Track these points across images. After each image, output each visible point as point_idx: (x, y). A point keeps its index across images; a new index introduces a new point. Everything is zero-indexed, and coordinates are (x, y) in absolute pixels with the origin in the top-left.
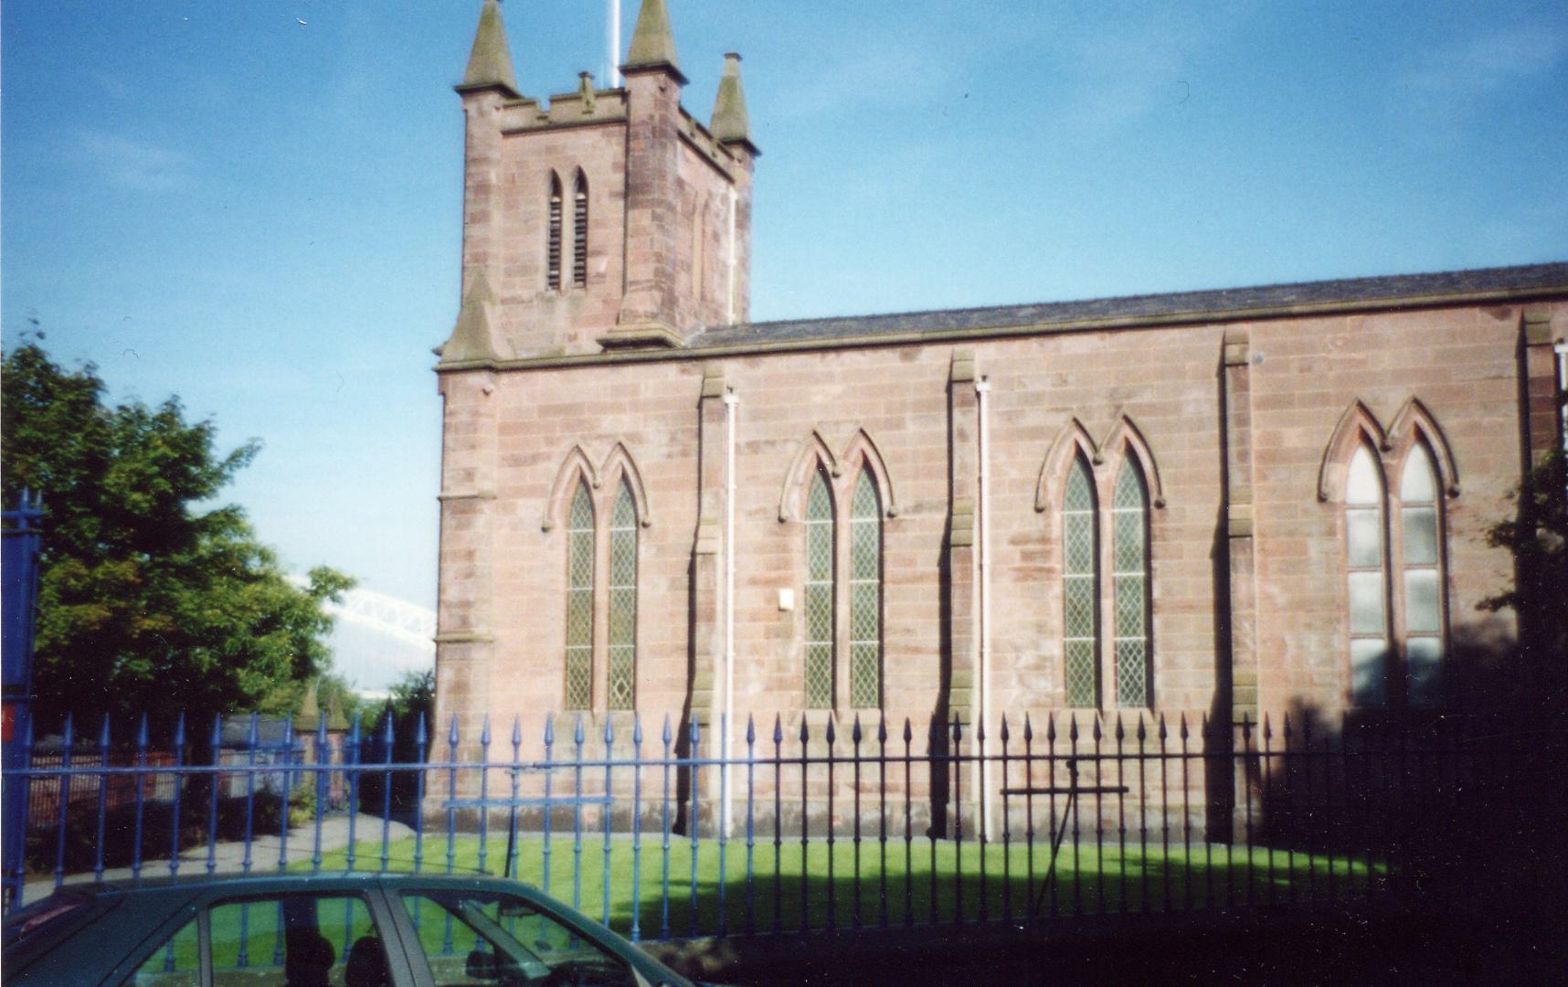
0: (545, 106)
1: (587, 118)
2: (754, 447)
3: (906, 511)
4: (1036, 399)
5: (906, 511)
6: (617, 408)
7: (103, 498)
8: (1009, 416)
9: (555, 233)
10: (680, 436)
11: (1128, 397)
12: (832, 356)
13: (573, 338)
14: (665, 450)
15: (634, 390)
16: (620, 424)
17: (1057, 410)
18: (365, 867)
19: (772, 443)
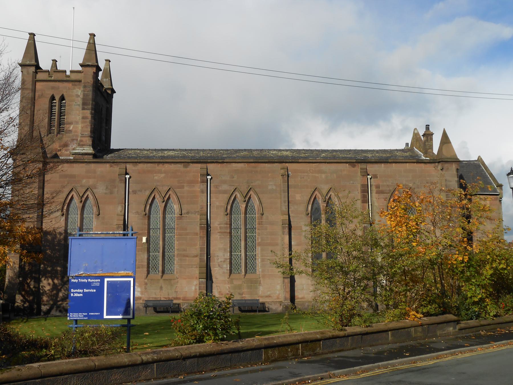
3: (184, 214)
4: (224, 182)
11: (252, 183)
12: (161, 165)
14: (105, 191)
19: (141, 191)
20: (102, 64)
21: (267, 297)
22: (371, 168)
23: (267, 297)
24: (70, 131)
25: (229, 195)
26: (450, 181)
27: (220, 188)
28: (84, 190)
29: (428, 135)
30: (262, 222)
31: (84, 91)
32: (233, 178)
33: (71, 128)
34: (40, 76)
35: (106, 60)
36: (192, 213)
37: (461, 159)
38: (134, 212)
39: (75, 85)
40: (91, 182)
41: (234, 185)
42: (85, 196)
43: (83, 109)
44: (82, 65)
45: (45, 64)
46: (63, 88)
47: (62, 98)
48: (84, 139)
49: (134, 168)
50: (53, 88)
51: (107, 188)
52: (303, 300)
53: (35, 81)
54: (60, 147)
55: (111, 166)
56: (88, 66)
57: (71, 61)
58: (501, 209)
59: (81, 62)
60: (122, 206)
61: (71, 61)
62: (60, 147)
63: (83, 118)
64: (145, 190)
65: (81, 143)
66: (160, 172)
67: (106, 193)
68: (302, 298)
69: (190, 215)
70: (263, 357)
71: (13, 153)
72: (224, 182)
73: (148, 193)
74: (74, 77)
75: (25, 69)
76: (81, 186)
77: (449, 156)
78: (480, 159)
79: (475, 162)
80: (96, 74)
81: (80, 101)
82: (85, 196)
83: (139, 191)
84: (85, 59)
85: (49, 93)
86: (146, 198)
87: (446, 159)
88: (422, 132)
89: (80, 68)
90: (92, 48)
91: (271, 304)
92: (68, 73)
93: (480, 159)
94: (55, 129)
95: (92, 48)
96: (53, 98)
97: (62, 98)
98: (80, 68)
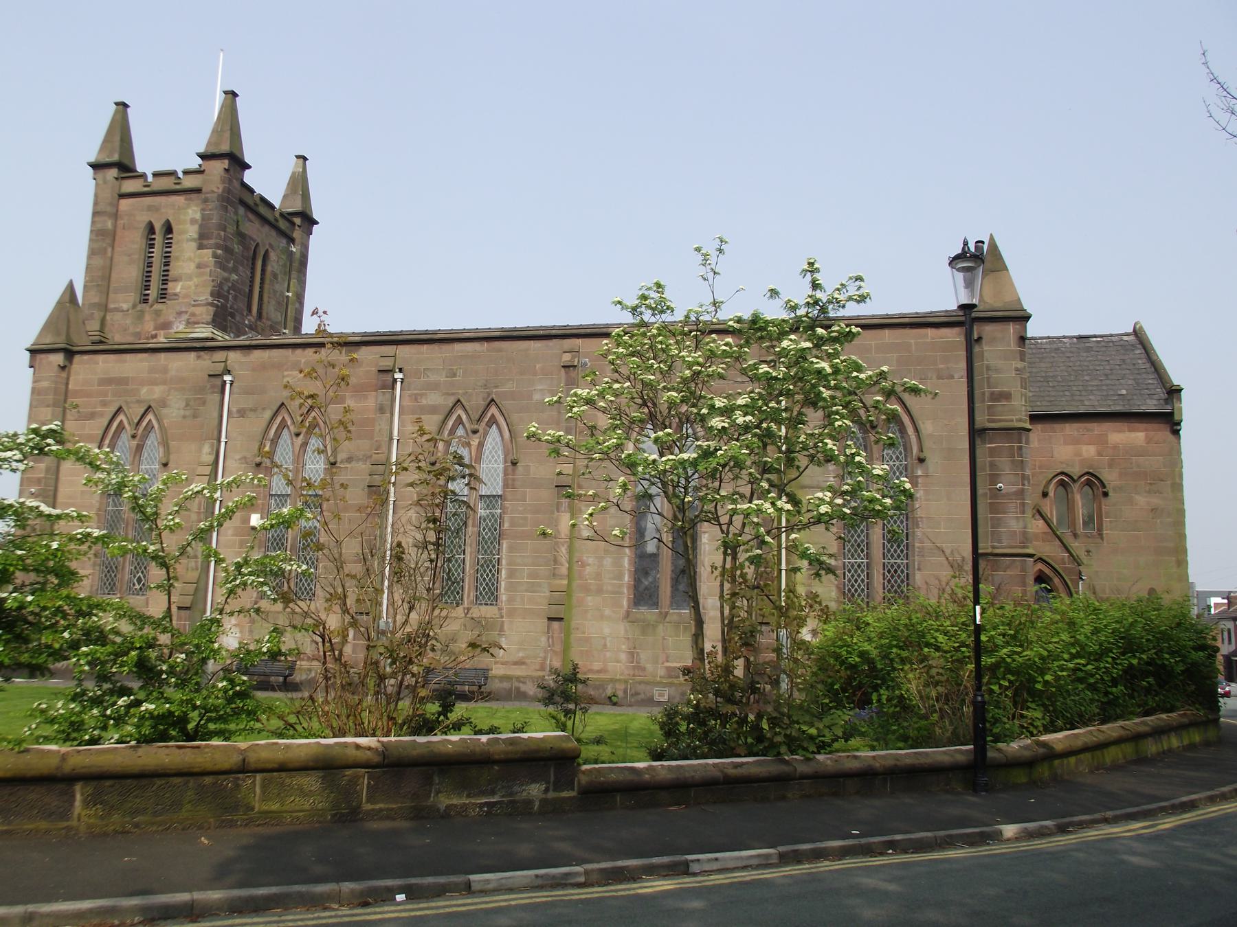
0: (150, 178)
1: (178, 187)
2: (242, 413)
3: (342, 462)
4: (435, 386)
5: (342, 462)
6: (153, 383)
7: (1214, 600)
8: (416, 398)
9: (261, 288)
10: (192, 403)
11: (496, 387)
12: (299, 351)
13: (155, 336)
14: (182, 412)
15: (165, 370)
16: (153, 393)
17: (447, 394)
18: (1164, 738)
19: (254, 410)
21: (515, 663)
23: (515, 663)
24: (176, 295)
25: (440, 417)
26: (997, 371)
27: (424, 402)
28: (142, 410)
30: (513, 480)
31: (203, 210)
32: (454, 375)
33: (178, 290)
35: (298, 157)
36: (359, 460)
38: (238, 457)
39: (190, 199)
40: (158, 392)
41: (453, 394)
42: (144, 424)
43: (200, 247)
44: (203, 157)
47: (169, 229)
48: (198, 310)
49: (244, 360)
50: (150, 208)
51: (187, 405)
52: (601, 676)
54: (156, 329)
55: (199, 357)
58: (1179, 453)
59: (202, 150)
60: (212, 445)
62: (156, 329)
63: (199, 266)
64: (264, 409)
65: (193, 319)
67: (184, 417)
68: (599, 672)
69: (354, 464)
72: (435, 386)
73: (268, 414)
74: (189, 182)
75: (101, 174)
76: (139, 402)
77: (998, 305)
79: (1125, 338)
81: (193, 231)
82: (144, 424)
83: (251, 410)
84: (209, 143)
85: (143, 219)
86: (264, 424)
91: (524, 683)
94: (153, 293)
96: (151, 229)
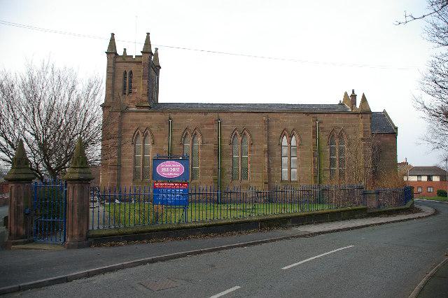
20: (153, 52)
22: (320, 117)
29: (354, 96)
34: (118, 60)
37: (373, 110)
45: (120, 52)
46: (133, 67)
53: (115, 62)
56: (146, 53)
57: (135, 50)
61: (135, 50)
66: (190, 118)
70: (285, 268)
71: (103, 106)
74: (137, 60)
78: (384, 112)
80: (150, 58)
87: (365, 111)
88: (350, 94)
89: (141, 54)
90: (148, 43)
92: (134, 57)
93: (384, 112)
95: (148, 43)
97: (131, 72)
98: (141, 54)
